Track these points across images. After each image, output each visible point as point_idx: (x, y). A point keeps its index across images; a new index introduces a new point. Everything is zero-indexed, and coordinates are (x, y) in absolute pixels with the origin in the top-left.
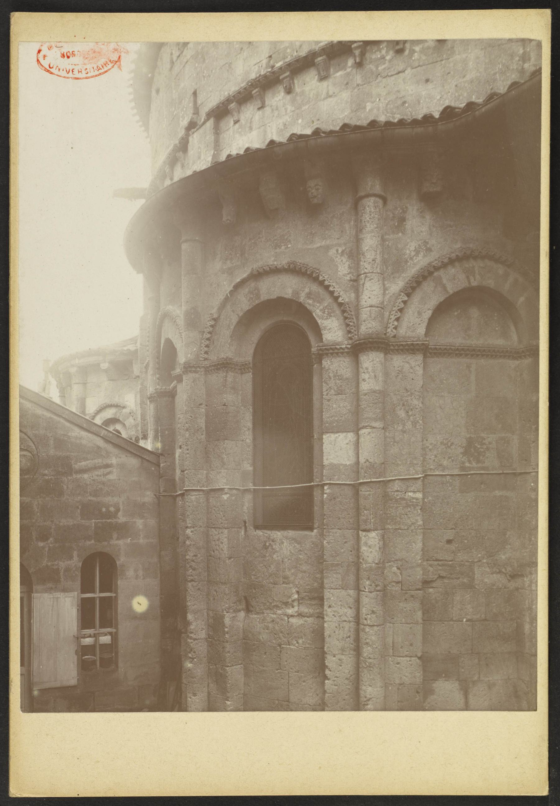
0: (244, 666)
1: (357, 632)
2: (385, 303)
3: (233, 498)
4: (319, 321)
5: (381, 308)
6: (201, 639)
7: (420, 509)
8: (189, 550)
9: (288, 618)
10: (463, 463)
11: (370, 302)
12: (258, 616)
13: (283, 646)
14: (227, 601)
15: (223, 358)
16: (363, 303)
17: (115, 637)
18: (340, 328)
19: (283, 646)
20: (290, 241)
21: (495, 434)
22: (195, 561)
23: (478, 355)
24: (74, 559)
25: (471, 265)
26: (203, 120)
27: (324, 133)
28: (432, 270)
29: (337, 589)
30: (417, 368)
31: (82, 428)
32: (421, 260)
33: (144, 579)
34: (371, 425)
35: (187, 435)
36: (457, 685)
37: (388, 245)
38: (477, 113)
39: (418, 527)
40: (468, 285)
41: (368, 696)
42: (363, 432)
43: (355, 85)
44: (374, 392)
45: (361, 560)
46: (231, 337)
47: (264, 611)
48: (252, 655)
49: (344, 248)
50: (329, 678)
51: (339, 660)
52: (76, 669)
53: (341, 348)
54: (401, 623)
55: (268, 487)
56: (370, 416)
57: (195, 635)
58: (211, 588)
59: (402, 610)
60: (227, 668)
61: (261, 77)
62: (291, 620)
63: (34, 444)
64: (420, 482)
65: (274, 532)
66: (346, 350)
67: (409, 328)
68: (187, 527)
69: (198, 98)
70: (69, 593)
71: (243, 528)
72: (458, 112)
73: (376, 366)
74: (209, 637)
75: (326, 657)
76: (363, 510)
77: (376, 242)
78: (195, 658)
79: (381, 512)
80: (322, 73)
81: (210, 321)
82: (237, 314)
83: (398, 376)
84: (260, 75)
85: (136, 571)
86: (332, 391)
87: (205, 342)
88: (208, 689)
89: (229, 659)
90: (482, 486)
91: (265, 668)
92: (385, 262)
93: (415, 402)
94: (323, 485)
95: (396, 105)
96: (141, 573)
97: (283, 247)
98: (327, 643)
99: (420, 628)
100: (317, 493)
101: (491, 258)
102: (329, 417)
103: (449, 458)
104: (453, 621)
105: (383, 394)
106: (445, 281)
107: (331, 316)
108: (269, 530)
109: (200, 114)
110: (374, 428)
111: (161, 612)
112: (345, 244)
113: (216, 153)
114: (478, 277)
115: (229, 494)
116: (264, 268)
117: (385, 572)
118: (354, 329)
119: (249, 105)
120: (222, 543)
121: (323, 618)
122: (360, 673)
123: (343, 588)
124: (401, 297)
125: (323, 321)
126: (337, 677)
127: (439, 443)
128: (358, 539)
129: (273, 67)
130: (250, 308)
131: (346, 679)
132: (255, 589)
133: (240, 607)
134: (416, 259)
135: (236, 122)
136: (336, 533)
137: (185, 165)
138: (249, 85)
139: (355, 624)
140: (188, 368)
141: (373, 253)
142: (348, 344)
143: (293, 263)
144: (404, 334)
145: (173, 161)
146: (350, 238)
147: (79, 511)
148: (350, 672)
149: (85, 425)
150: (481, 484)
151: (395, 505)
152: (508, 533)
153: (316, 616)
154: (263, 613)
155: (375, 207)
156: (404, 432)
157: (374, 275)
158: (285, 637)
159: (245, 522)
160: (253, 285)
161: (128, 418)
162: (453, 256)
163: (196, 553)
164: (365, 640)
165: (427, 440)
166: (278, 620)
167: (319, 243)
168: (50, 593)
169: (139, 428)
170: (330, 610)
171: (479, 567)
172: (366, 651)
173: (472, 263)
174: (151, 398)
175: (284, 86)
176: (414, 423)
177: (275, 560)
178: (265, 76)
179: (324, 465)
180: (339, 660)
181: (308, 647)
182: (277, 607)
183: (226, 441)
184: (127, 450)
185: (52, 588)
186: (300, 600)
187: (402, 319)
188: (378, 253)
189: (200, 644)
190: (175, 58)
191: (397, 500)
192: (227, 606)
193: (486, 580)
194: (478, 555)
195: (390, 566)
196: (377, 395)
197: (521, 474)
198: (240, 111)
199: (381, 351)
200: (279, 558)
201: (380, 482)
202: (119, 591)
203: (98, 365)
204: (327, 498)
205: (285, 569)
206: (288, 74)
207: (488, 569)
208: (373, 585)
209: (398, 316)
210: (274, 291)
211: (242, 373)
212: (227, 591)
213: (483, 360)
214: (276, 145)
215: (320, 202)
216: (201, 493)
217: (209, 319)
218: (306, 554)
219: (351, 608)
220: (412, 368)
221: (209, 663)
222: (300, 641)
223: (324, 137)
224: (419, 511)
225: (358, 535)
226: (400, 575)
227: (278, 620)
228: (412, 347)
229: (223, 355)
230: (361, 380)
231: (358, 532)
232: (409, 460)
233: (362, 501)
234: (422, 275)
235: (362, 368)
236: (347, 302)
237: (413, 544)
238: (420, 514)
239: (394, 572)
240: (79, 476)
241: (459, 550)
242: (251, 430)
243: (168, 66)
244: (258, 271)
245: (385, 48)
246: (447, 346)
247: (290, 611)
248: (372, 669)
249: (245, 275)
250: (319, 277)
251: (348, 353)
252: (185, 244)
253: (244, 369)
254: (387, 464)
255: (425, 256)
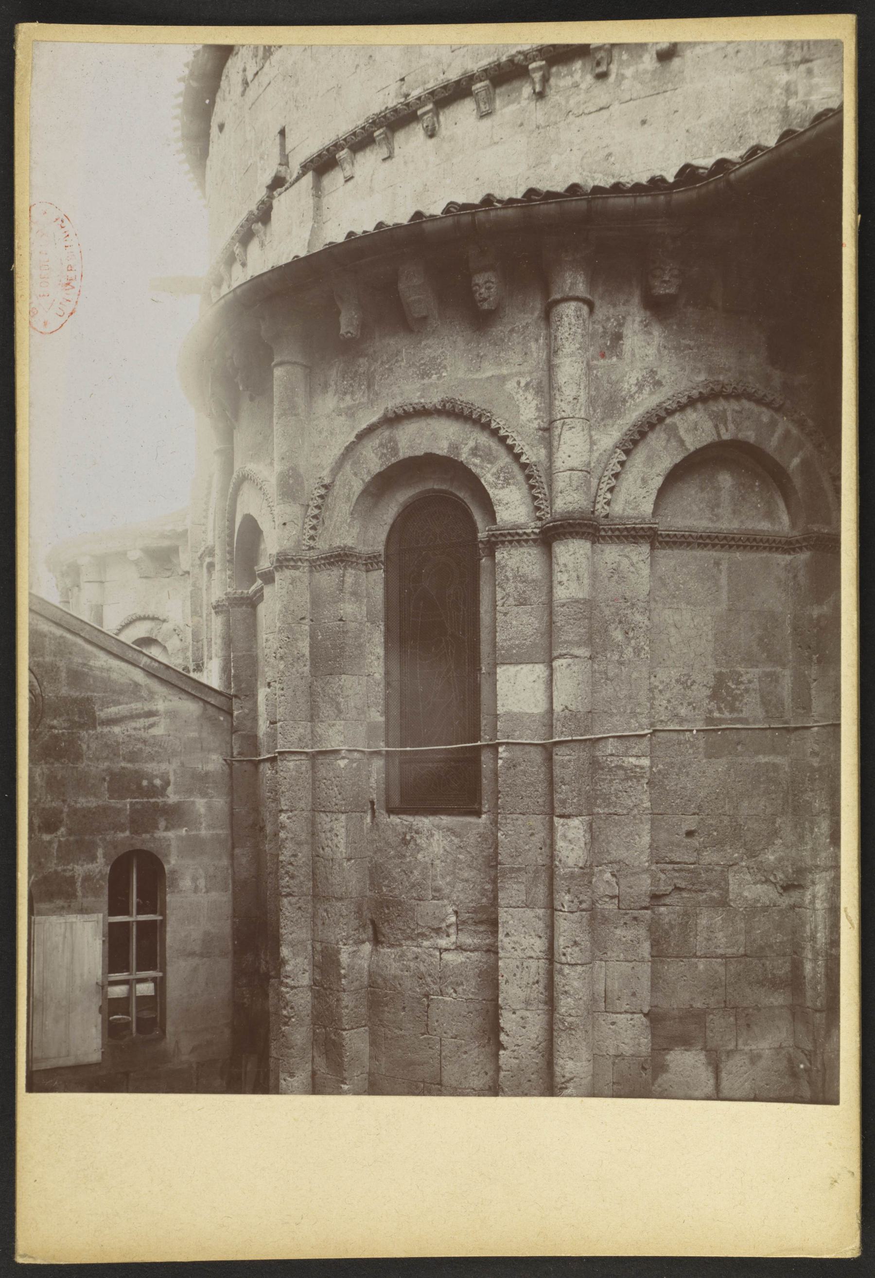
0: (370, 1029)
1: (550, 974)
2: (592, 465)
3: (355, 765)
4: (491, 492)
5: (586, 471)
6: (302, 986)
7: (647, 783)
8: (284, 847)
9: (441, 954)
10: (711, 712)
11: (570, 463)
12: (393, 951)
13: (432, 997)
14: (344, 927)
15: (339, 547)
16: (558, 464)
17: (160, 984)
18: (524, 503)
19: (432, 997)
20: (445, 367)
21: (757, 667)
22: (295, 863)
23: (731, 547)
24: (98, 860)
25: (721, 408)
26: (295, 176)
27: (499, 201)
28: (663, 414)
29: (518, 907)
30: (641, 565)
31: (110, 653)
32: (646, 399)
33: (207, 892)
34: (571, 652)
35: (282, 667)
36: (704, 1057)
37: (596, 375)
38: (732, 176)
39: (644, 811)
40: (717, 439)
41: (568, 1075)
42: (560, 664)
43: (535, 127)
44: (577, 601)
45: (557, 863)
46: (352, 514)
47: (403, 942)
48: (383, 1011)
49: (528, 379)
50: (505, 1046)
51: (522, 1018)
52: (100, 1036)
53: (525, 533)
54: (617, 961)
55: (408, 749)
56: (570, 638)
57: (293, 980)
58: (318, 906)
59: (620, 939)
60: (344, 1033)
61: (388, 111)
62: (446, 956)
63: (36, 678)
64: (645, 741)
65: (418, 818)
66: (533, 537)
67: (627, 502)
68: (281, 811)
69: (287, 139)
70: (89, 915)
71: (369, 812)
72: (703, 173)
73: (579, 561)
74: (314, 983)
75: (501, 1014)
76: (560, 784)
77: (579, 371)
78: (293, 1017)
79: (588, 788)
80: (482, 106)
81: (319, 488)
82: (362, 479)
83: (612, 577)
84: (387, 108)
85: (194, 879)
86: (511, 599)
87: (310, 521)
88: (312, 1065)
89: (346, 1018)
90: (739, 747)
91: (403, 1032)
92: (592, 401)
93: (638, 617)
94: (495, 747)
95: (597, 159)
96: (202, 883)
97: (434, 376)
98: (502, 992)
99: (647, 968)
100: (486, 757)
101: (750, 397)
102: (505, 640)
103: (689, 704)
104: (697, 957)
105: (590, 604)
106: (682, 433)
107: (509, 484)
108: (410, 814)
109: (290, 164)
110: (576, 657)
111: (234, 944)
112: (530, 373)
113: (316, 226)
114: (731, 427)
115: (348, 759)
116: (405, 408)
117: (594, 880)
118: (545, 503)
119: (368, 151)
120: (337, 836)
121: (497, 953)
122: (555, 1039)
123: (527, 906)
124: (616, 455)
125: (496, 492)
126: (518, 1045)
127: (673, 681)
128: (552, 829)
129: (407, 96)
130: (382, 469)
131: (533, 1048)
132: (388, 908)
133: (364, 936)
134: (639, 397)
135: (348, 179)
136: (517, 820)
137: (266, 243)
138: (370, 123)
139: (547, 961)
140: (284, 561)
141: (575, 387)
142: (535, 528)
143: (451, 400)
144: (621, 512)
145: (246, 236)
146: (539, 363)
147: (106, 784)
148: (538, 1037)
149: (115, 649)
150: (738, 745)
151: (608, 777)
152: (779, 820)
153: (484, 949)
154: (401, 945)
155: (578, 317)
156: (621, 663)
157: (577, 421)
158: (435, 983)
159: (372, 803)
160: (387, 433)
161: (170, 637)
162: (695, 393)
163: (295, 850)
164: (563, 987)
165: (655, 677)
166: (425, 956)
167: (489, 371)
168: (61, 915)
169: (189, 654)
170: (509, 941)
171: (735, 873)
172: (565, 1004)
173: (721, 405)
174: (218, 608)
175: (425, 125)
176: (637, 651)
177: (420, 862)
178: (395, 110)
179: (498, 715)
180: (522, 1018)
181: (472, 999)
182: (422, 935)
183: (343, 676)
184: (183, 690)
185: (63, 908)
186: (460, 926)
187: (617, 489)
188: (582, 387)
189: (301, 995)
190: (250, 77)
191: (610, 770)
192: (344, 934)
193: (746, 894)
194: (733, 855)
195: (601, 871)
196: (581, 606)
197: (796, 729)
198: (355, 162)
199: (586, 539)
200: (427, 859)
201: (585, 740)
202: (167, 912)
203: (125, 554)
204: (503, 765)
205: (436, 876)
206: (430, 106)
207: (748, 877)
208: (576, 900)
209: (612, 485)
210: (420, 444)
211: (367, 571)
212: (345, 913)
213: (738, 554)
214: (424, 219)
215: (493, 308)
216: (303, 758)
217: (317, 485)
218: (469, 853)
219: (540, 937)
220: (632, 565)
221: (314, 1024)
222: (460, 989)
223: (500, 208)
224: (645, 785)
225: (552, 822)
226: (616, 886)
227: (425, 956)
228: (633, 533)
229: (337, 542)
230: (555, 583)
231: (552, 819)
232: (629, 708)
233: (557, 771)
234: (648, 423)
235: (558, 564)
236: (535, 462)
237: (637, 837)
238: (646, 791)
239: (607, 881)
240: (106, 730)
241: (705, 847)
242: (382, 660)
243: (240, 89)
244: (395, 412)
245: (580, 71)
246: (685, 531)
247: (443, 942)
248: (573, 1032)
249: (374, 419)
250: (491, 423)
251: (534, 541)
252: (280, 369)
253: (372, 564)
254: (596, 713)
255: (652, 393)
